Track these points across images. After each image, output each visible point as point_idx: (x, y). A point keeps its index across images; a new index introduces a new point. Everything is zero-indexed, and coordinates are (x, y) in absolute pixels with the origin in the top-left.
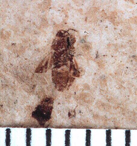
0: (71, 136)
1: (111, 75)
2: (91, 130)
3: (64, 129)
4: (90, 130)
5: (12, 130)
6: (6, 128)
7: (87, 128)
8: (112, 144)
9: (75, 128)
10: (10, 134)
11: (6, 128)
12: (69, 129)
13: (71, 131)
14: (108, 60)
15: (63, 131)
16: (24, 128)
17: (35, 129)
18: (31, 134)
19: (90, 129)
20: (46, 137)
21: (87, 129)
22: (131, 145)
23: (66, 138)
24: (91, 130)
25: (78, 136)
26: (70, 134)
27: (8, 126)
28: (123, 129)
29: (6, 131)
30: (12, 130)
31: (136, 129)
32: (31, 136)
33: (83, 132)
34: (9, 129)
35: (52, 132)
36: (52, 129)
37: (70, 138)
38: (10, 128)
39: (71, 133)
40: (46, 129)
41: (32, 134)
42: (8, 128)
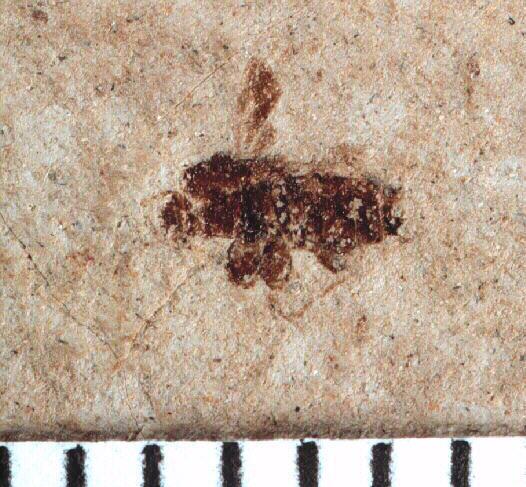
0: (393, 466)
2: (469, 440)
5: (168, 448)
12: (386, 441)
13: (394, 447)
15: (364, 448)
18: (239, 464)
21: (455, 439)
23: (374, 476)
26: (388, 459)
29: (143, 457)
30: (168, 448)
31: (521, 434)
34: (156, 448)
35: (322, 455)
37: (390, 476)
39: (393, 455)
41: (243, 464)
42: (152, 442)
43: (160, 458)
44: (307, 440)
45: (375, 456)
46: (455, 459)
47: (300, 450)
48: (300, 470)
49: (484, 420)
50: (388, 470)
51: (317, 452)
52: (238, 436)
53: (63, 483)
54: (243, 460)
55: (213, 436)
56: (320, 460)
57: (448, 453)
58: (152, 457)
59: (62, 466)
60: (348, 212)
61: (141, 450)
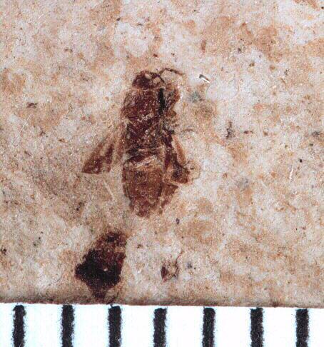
0: (167, 323)
1: (262, 177)
2: (215, 308)
3: (151, 306)
4: (212, 310)
5: (29, 308)
6: (14, 305)
7: (207, 305)
8: (265, 343)
9: (178, 304)
10: (24, 317)
11: (14, 305)
12: (163, 307)
13: (168, 311)
14: (255, 143)
15: (148, 312)
16: (58, 304)
17: (83, 306)
18: (73, 319)
19: (214, 305)
20: (108, 326)
21: (206, 307)
22: (309, 345)
23: (155, 328)
24: (215, 308)
25: (184, 324)
26: (165, 318)
27: (20, 300)
28: (292, 306)
29: (14, 312)
30: (29, 308)
31: (321, 307)
32: (74, 323)
33: (197, 313)
34: (22, 307)
35: (123, 315)
36: (123, 307)
37: (165, 329)
38: (25, 305)
39: (167, 316)
40: (109, 306)
41: (75, 319)
42: (20, 304)
43: (24, 313)
44: (115, 305)
45: (156, 316)
46: (252, 318)
47: (110, 311)
48: (110, 323)
49: (287, 299)
50: (164, 325)
51: (120, 313)
52: (71, 302)
53: (152, 344)
54: (75, 316)
55: (198, 303)
56: (122, 317)
57: (201, 315)
58: (160, 318)
59: (310, 338)
60: (151, 104)
61: (13, 308)
